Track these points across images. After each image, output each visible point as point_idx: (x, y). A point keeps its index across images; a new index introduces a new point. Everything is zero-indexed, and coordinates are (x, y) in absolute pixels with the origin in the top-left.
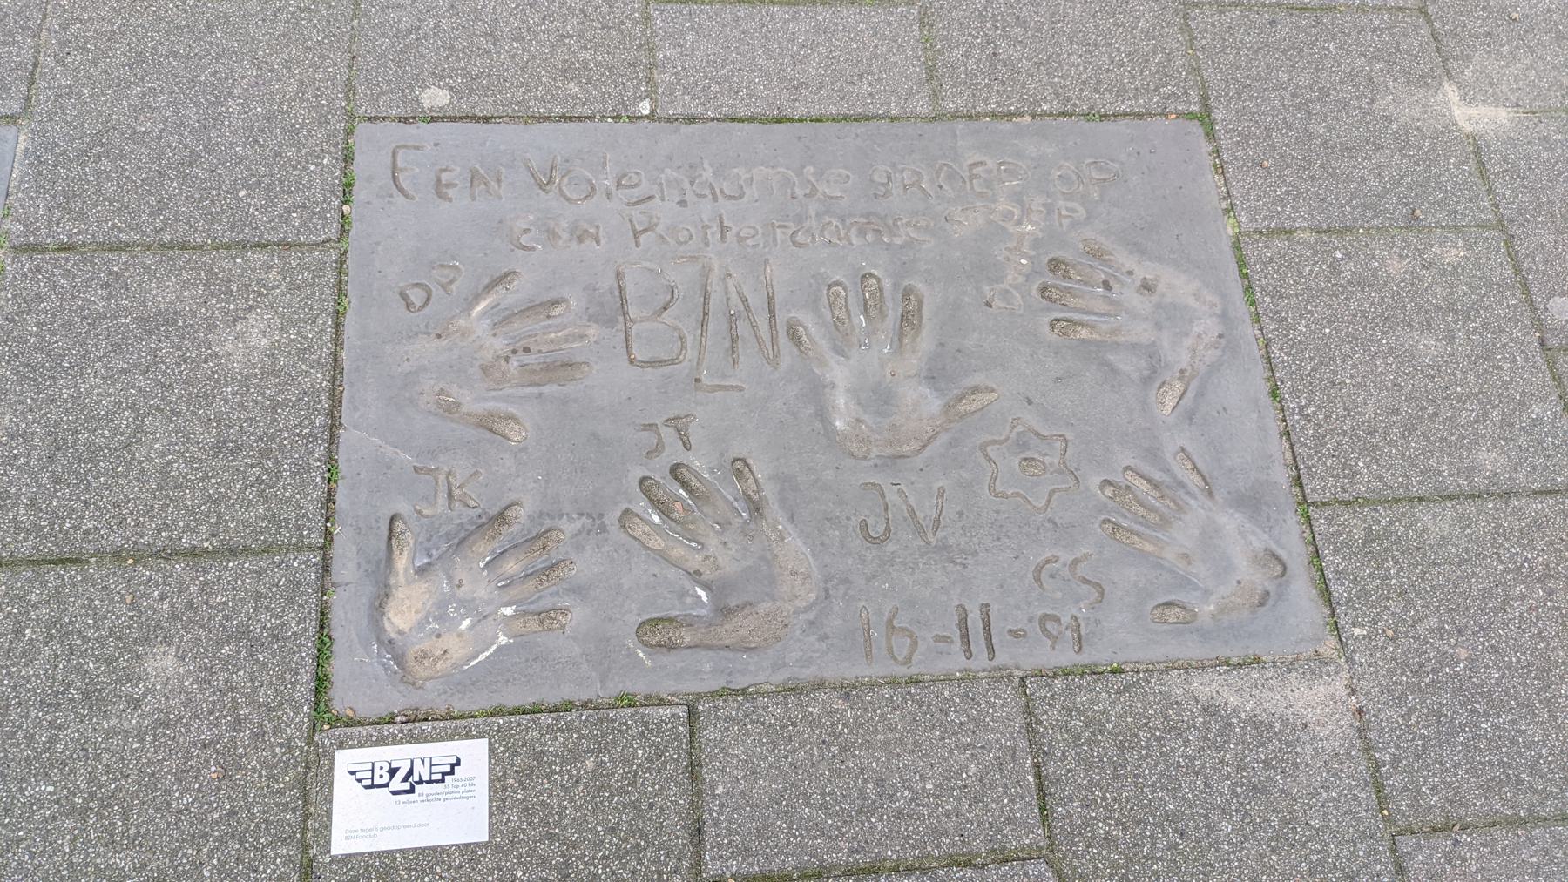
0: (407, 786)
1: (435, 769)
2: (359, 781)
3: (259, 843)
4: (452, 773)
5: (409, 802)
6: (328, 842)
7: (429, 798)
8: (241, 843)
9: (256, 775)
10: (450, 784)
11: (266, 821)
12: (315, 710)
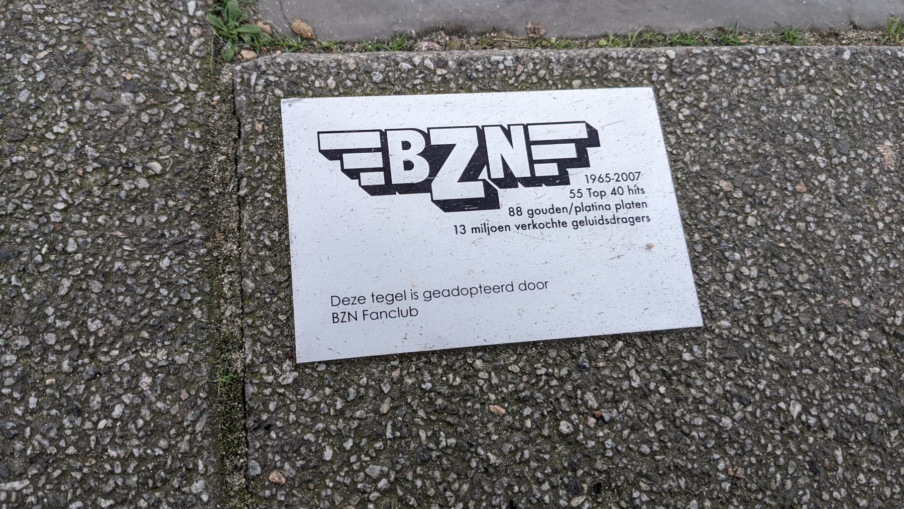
0: (475, 190)
1: (539, 152)
2: (353, 174)
3: (85, 331)
4: (582, 161)
5: (487, 229)
6: (287, 328)
7: (538, 219)
8: (33, 334)
9: (69, 157)
10: (584, 186)
11: (106, 276)
12: (218, 13)
